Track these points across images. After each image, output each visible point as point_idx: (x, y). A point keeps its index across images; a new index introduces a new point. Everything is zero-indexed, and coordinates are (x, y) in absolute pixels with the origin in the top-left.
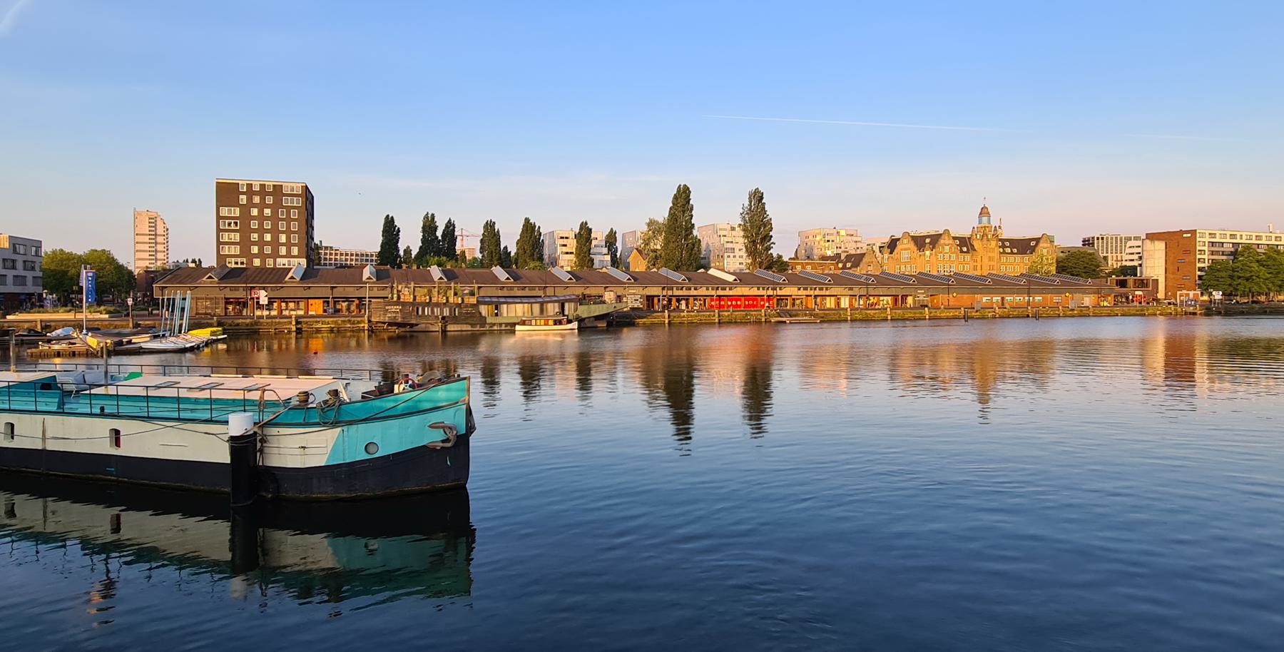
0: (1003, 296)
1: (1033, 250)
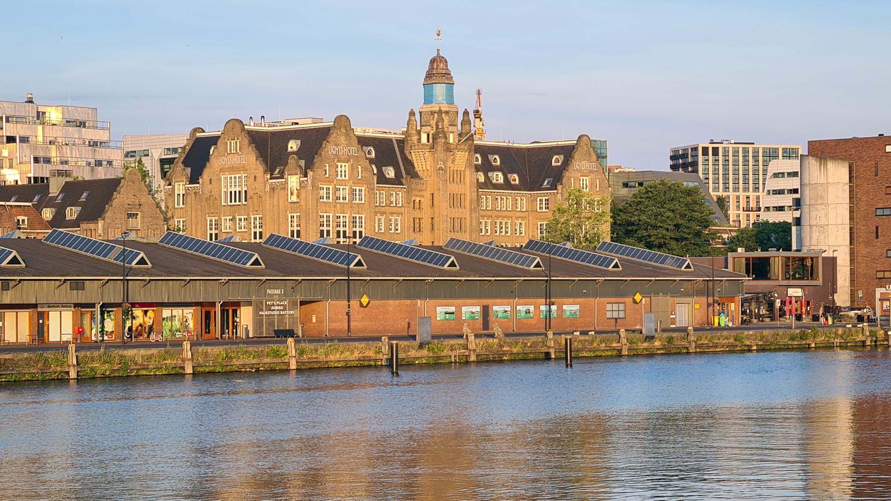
1: (557, 177)
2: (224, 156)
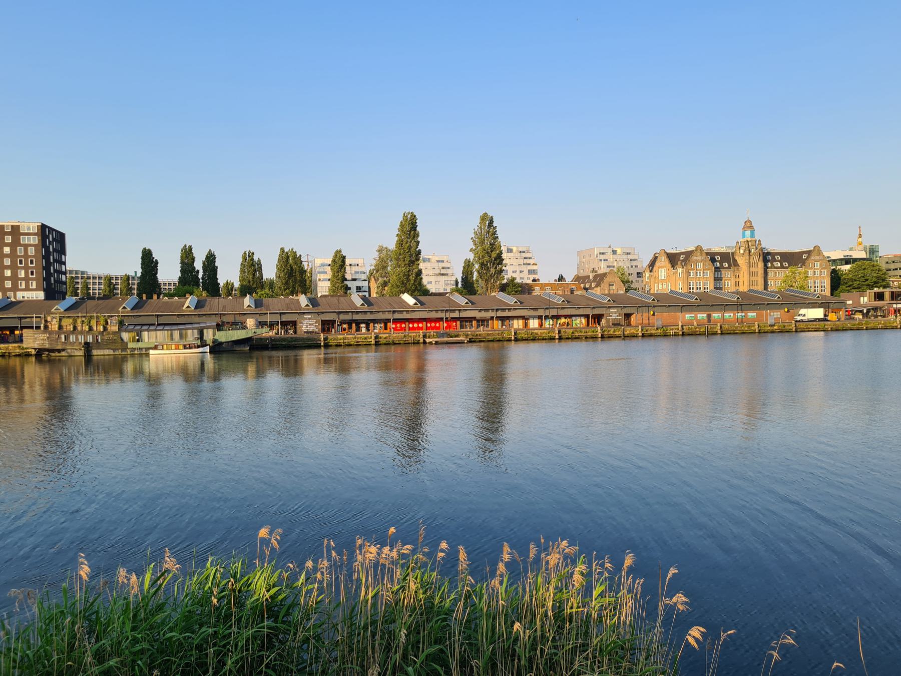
0: (709, 313)
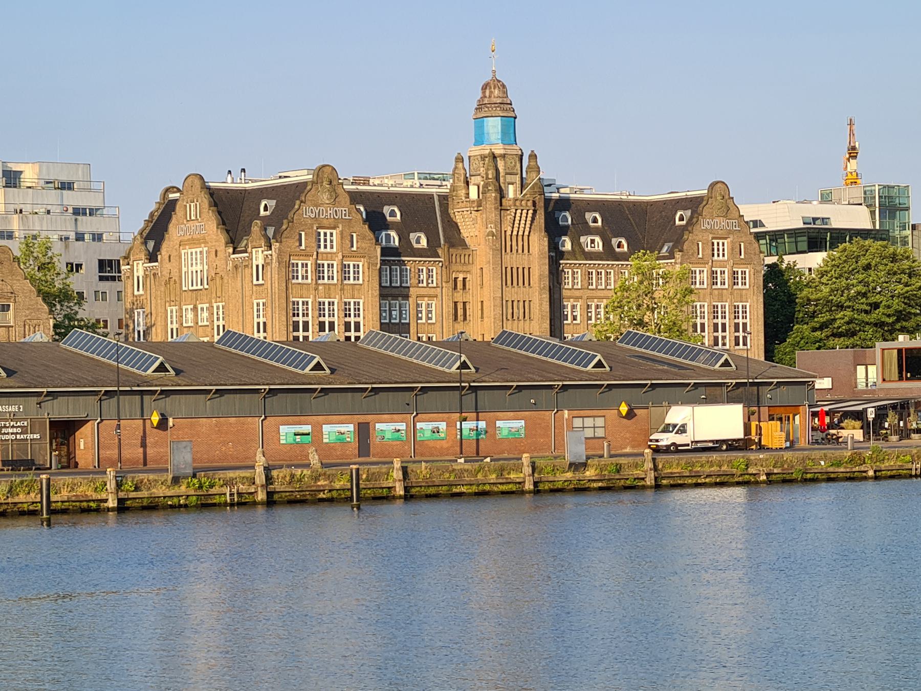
1: (678, 239)
2: (183, 223)
